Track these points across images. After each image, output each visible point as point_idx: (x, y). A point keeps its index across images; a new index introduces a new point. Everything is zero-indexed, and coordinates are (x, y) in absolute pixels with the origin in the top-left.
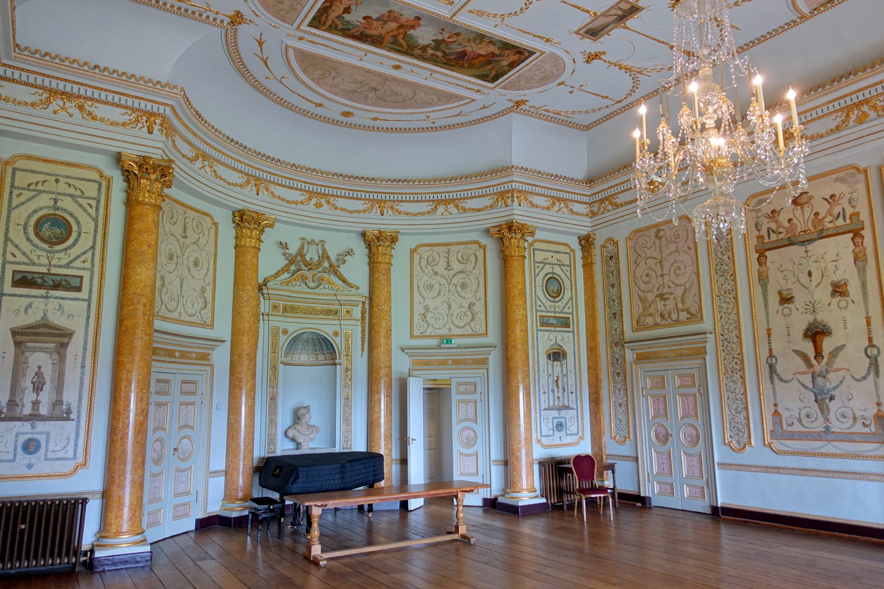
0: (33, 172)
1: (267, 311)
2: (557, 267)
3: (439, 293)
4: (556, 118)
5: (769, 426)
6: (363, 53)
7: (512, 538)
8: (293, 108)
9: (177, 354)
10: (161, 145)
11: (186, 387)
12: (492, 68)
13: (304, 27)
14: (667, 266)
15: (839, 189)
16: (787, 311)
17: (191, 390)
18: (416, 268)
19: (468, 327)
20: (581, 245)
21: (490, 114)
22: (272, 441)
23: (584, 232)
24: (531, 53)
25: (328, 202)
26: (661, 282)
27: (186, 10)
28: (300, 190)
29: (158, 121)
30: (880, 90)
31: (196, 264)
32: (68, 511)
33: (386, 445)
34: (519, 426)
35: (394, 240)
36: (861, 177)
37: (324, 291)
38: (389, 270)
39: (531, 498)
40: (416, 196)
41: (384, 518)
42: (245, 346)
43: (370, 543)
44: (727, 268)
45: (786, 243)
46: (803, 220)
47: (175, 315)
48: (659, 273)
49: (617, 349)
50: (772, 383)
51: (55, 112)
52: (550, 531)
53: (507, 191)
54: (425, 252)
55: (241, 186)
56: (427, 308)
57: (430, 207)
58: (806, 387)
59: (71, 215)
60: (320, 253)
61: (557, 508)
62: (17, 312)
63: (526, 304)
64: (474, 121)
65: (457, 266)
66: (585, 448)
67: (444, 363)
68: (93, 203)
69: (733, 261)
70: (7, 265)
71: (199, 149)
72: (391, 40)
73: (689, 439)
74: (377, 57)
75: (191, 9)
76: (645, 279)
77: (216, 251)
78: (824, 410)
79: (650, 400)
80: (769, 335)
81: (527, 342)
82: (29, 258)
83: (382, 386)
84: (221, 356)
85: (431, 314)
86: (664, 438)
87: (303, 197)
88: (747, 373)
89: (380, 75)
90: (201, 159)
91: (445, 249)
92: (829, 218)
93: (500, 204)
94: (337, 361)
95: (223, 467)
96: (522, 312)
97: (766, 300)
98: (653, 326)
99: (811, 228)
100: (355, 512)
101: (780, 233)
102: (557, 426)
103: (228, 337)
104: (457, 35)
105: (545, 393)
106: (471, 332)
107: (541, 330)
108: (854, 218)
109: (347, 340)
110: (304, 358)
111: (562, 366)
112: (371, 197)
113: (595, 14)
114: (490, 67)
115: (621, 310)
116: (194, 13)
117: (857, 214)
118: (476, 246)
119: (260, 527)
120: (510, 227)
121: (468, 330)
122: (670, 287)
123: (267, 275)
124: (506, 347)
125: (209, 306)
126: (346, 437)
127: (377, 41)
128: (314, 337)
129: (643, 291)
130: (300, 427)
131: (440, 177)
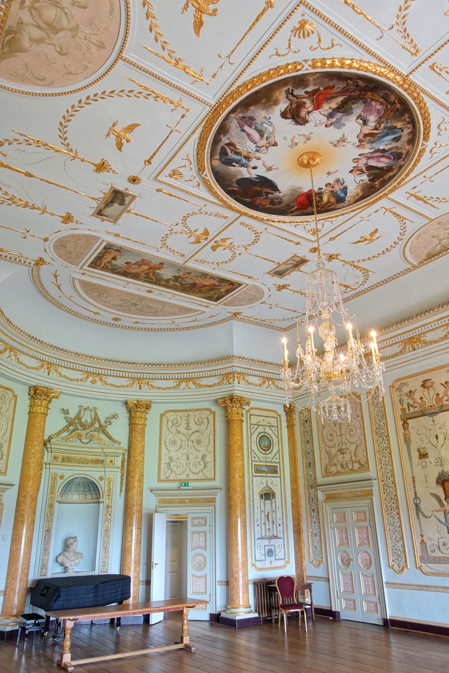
1: (49, 461)
2: (268, 428)
3: (180, 447)
4: (263, 324)
5: (419, 553)
6: (126, 283)
7: (231, 648)
8: (78, 315)
12: (215, 293)
13: (85, 267)
16: (424, 464)
18: (164, 428)
19: (201, 473)
20: (285, 411)
21: (217, 320)
22: (44, 566)
24: (240, 285)
25: (101, 380)
27: (6, 257)
30: (447, 322)
33: (135, 568)
34: (237, 552)
35: (148, 407)
37: (94, 445)
38: (144, 429)
40: (165, 376)
42: (29, 489)
43: (117, 651)
44: (383, 431)
45: (420, 414)
46: (429, 398)
49: (312, 491)
50: (418, 518)
52: (262, 640)
53: (230, 373)
54: (171, 416)
55: (37, 369)
56: (171, 459)
57: (175, 384)
58: (441, 522)
61: (268, 621)
63: (243, 455)
64: (206, 325)
65: (194, 427)
66: (290, 571)
67: (182, 501)
69: (387, 426)
71: (8, 344)
72: (145, 276)
73: (365, 563)
74: (136, 286)
76: (330, 438)
77: (14, 416)
79: (336, 531)
81: (244, 485)
83: (134, 520)
86: (347, 562)
87: (82, 376)
89: (139, 296)
90: (8, 351)
91: (186, 414)
93: (225, 382)
94: (100, 500)
96: (240, 462)
97: (410, 455)
98: (336, 473)
99: (435, 404)
100: (108, 627)
101: (416, 407)
103: (16, 481)
104: (189, 273)
105: (258, 525)
106: (203, 477)
107: (256, 476)
109: (109, 483)
110: (75, 497)
111: (271, 504)
112: (133, 376)
113: (279, 263)
114: (213, 292)
115: (314, 461)
116: (11, 258)
118: (208, 412)
119: (26, 639)
120: (231, 398)
121: (201, 476)
122: (346, 444)
123: (51, 433)
124: (229, 489)
125: (5, 457)
127: (136, 276)
128: (85, 481)
129: (329, 447)
130: (68, 554)
131: (183, 362)
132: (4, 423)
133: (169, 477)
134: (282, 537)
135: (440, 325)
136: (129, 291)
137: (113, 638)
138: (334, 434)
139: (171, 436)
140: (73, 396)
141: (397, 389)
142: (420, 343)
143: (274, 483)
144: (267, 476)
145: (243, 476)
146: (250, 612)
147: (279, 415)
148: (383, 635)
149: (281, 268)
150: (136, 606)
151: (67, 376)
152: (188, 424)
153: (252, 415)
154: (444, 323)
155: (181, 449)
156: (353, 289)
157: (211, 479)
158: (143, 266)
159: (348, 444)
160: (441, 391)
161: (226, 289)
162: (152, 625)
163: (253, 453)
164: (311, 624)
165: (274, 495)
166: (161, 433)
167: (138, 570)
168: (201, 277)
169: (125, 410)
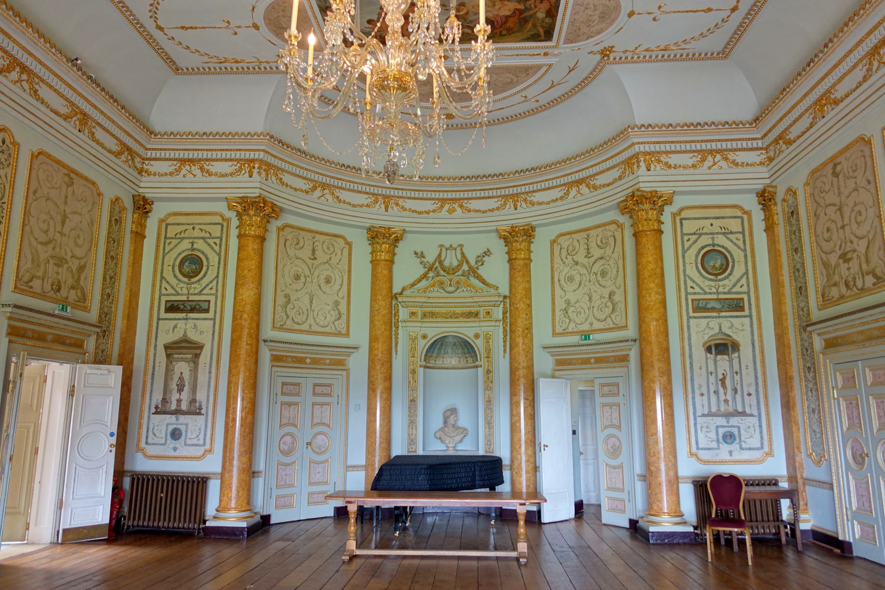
0: (178, 224)
2: (721, 236)
3: (580, 285)
9: (308, 361)
10: (258, 185)
11: (319, 390)
12: (534, 26)
14: (847, 211)
17: (325, 392)
18: (557, 260)
25: (461, 206)
26: (843, 237)
29: (257, 166)
31: (328, 281)
32: (196, 485)
37: (462, 294)
47: (305, 327)
48: (840, 224)
49: (805, 336)
51: (184, 176)
54: (565, 242)
56: (568, 303)
59: (203, 253)
62: (167, 332)
65: (596, 253)
66: (775, 467)
68: (218, 241)
70: (162, 297)
75: (251, 66)
76: (826, 235)
82: (702, 289)
84: (359, 363)
90: (319, 189)
91: (584, 234)
95: (364, 463)
102: (725, 437)
105: (702, 395)
106: (612, 326)
107: (695, 318)
110: (454, 361)
111: (731, 361)
114: (530, 25)
118: (613, 227)
121: (609, 324)
122: (852, 242)
125: (344, 317)
129: (826, 253)
132: (338, 277)
133: (567, 328)
134: (755, 413)
138: (833, 226)
139: (566, 269)
140: (427, 236)
143: (736, 327)
144: (719, 317)
152: (588, 249)
153: (685, 219)
157: (622, 327)
159: (855, 240)
161: (544, 10)
162: (545, 524)
163: (688, 281)
166: (552, 268)
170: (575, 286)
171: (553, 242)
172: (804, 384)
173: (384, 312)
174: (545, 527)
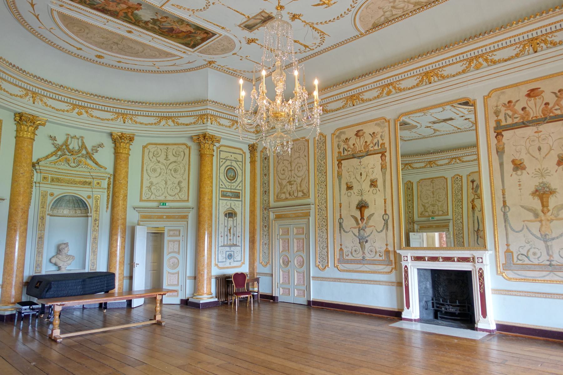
1: (39, 180)
2: (234, 162)
3: (160, 174)
5: (337, 257)
6: (106, 21)
7: (196, 324)
8: (60, 49)
12: (191, 40)
15: (377, 129)
16: (349, 194)
18: (146, 158)
21: (194, 67)
23: (252, 142)
24: (214, 34)
25: (87, 112)
28: (67, 102)
34: (204, 256)
35: (131, 139)
36: (387, 124)
38: (128, 158)
39: (208, 298)
40: (147, 113)
41: (117, 313)
42: (20, 203)
43: (104, 326)
46: (359, 144)
48: (289, 169)
49: (265, 212)
50: (340, 233)
53: (204, 115)
54: (152, 148)
55: (21, 97)
56: (152, 183)
57: (156, 120)
58: (355, 235)
60: (80, 144)
61: (225, 304)
63: (212, 183)
65: (172, 158)
66: (245, 269)
67: (161, 217)
72: (124, 15)
76: (282, 172)
78: (363, 247)
79: (281, 241)
80: (340, 207)
81: (212, 206)
83: (119, 230)
85: (154, 187)
86: (286, 263)
88: (329, 227)
89: (119, 35)
91: (165, 147)
92: (372, 145)
97: (340, 187)
98: (285, 199)
100: (97, 310)
102: (228, 256)
104: (167, 17)
105: (222, 236)
106: (178, 199)
108: (382, 146)
109: (97, 201)
110: (66, 212)
113: (248, 17)
114: (189, 39)
115: (269, 190)
117: (384, 143)
118: (184, 147)
120: (204, 136)
126: (93, 263)
127: (114, 14)
128: (74, 199)
130: (60, 256)
131: (164, 102)
133: (150, 198)
135: (376, 86)
136: (110, 29)
137: (101, 318)
138: (286, 169)
139: (152, 164)
140: (58, 125)
141: (337, 136)
142: (359, 100)
143: (236, 205)
145: (212, 199)
146: (211, 298)
147: (244, 153)
148: (306, 311)
149: (251, 22)
150: (121, 294)
151: (53, 106)
152: (167, 155)
154: (378, 85)
155: (161, 176)
156: (311, 50)
158: (121, 5)
160: (369, 139)
161: (202, 37)
164: (256, 305)
165: (235, 214)
167: (122, 268)
168: (178, 22)
169: (110, 141)
170: (157, 175)
171: (144, 147)
172: (262, 232)
173: (28, 175)
174: (164, 306)
